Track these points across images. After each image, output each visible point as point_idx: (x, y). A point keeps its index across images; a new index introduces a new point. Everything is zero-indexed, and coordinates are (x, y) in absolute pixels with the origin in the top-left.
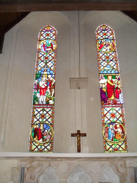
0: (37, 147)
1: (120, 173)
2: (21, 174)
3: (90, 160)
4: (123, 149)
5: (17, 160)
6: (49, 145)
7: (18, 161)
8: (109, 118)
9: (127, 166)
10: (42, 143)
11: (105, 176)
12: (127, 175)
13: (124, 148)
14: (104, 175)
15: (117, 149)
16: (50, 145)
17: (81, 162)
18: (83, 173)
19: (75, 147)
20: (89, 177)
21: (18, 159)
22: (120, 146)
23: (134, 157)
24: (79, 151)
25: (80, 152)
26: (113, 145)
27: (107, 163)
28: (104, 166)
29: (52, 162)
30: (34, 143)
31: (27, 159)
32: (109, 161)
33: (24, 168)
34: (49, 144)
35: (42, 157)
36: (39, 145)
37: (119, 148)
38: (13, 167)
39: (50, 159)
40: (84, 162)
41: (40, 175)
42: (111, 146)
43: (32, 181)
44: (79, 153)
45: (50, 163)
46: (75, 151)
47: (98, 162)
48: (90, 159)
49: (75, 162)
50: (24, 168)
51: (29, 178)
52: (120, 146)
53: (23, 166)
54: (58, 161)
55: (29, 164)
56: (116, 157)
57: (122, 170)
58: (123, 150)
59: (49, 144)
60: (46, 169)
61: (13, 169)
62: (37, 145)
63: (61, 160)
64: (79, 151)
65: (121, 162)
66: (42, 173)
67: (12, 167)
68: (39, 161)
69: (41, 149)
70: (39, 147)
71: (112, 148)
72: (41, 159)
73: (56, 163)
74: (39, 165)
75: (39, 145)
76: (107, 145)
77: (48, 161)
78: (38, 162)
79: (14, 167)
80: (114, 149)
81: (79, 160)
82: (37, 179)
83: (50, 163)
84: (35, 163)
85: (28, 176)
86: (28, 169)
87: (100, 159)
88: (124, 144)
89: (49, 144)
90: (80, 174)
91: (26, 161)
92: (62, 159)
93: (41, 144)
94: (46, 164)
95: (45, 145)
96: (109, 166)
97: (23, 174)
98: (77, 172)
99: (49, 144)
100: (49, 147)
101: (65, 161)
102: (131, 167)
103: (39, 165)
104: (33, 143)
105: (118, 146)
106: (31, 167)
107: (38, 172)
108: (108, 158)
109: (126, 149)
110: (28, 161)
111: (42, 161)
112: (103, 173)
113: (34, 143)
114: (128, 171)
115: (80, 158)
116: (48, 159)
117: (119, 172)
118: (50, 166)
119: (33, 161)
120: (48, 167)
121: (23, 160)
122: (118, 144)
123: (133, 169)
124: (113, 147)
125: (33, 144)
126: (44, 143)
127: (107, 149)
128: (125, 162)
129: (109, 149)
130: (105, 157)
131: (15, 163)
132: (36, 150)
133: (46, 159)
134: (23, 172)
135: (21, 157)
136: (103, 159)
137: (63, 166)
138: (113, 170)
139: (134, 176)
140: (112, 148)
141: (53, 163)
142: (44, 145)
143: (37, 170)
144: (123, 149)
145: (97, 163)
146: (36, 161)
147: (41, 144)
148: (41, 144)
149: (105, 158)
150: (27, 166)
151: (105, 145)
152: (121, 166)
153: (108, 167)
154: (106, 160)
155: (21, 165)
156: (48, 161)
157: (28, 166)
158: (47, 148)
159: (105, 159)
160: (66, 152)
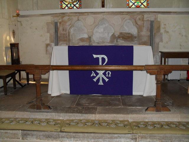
0: (67, 5)
1: (138, 25)
2: (55, 28)
3: (113, 14)
4: (144, 6)
5: (50, 17)
6: (77, 3)
7: (52, 17)
8: (142, 5)
9: (145, 19)
10: (71, 1)
11: (126, 27)
12: (144, 26)
13: (146, 6)
14: (124, 27)
15: (139, 6)
16: (78, 3)
17: (105, 16)
18: (107, 25)
19: (100, 3)
20: (112, 28)
21: (51, 15)
22: (142, 4)
23: (151, 12)
24: (103, 6)
25: (104, 7)
26: (135, 2)
27: (128, 17)
28: (125, 19)
29: (80, 17)
30: (64, 2)
31: (58, 15)
32: (129, 15)
33: (57, 23)
34: (77, 2)
35: (71, 13)
36: (68, 4)
37: (141, 5)
38: (48, 23)
39: (78, 14)
40: (107, 16)
41: (71, 27)
42: (134, 4)
43: (64, 32)
44: (103, 8)
45: (78, 17)
46: (100, 7)
47: (120, 16)
48: (112, 13)
49: (100, 16)
50: (57, 23)
51: (62, 30)
52: (142, 4)
53: (56, 21)
54: (85, 15)
55: (61, 19)
56: (135, 12)
57: (140, 23)
58: (144, 7)
59: (77, 2)
60: (76, 23)
61: (48, 24)
62: (67, 4)
63: (88, 15)
64: (103, 6)
65: (140, 16)
66: (72, 26)
67: (47, 23)
68: (69, 16)
69: (71, 7)
70: (69, 5)
71: (135, 5)
72: (71, 14)
73: (84, 17)
74: (69, 20)
75: (68, 4)
76: (130, 2)
77: (77, 16)
78: (68, 17)
79: (49, 22)
80: (137, 6)
81: (103, 14)
82: (69, 31)
83: (78, 17)
84: (66, 18)
85: (61, 29)
86: (60, 23)
87: (121, 13)
88: (146, 2)
89: (78, 2)
90: (104, 26)
91: (58, 17)
92: (89, 14)
93: (71, 3)
94: (75, 18)
95: (74, 4)
96: (129, 19)
97: (56, 27)
98: (102, 25)
99: (78, 2)
100: (77, 5)
101: (91, 15)
102: (148, 21)
103: (69, 20)
104: (63, 3)
105: (140, 4)
106: (62, 21)
107: (69, 25)
108: (128, 13)
109: (148, 6)
110: (59, 17)
111: (72, 16)
112: (123, 25)
113: (64, 2)
114: (145, 24)
115: (104, 12)
116: (77, 14)
117: (137, 24)
118: (78, 20)
119: (64, 17)
120: (77, 21)
121: (56, 16)
122: (140, 2)
123: (150, 22)
124: (136, 4)
125: (63, 3)
126: (72, 2)
127: (130, 6)
128: (143, 16)
129: (132, 6)
130: (125, 12)
131: (49, 19)
132: (67, 8)
133: (75, 14)
134: (56, 26)
135: (53, 14)
136: (124, 13)
137: (90, 20)
138: (133, 23)
139: (150, 27)
140: (135, 5)
141: (81, 17)
142: (73, 4)
143: (68, 24)
144: (144, 6)
145: (119, 17)
146: (66, 16)
147: (71, 3)
148: (70, 2)
149: (126, 12)
150: (60, 21)
151: (129, 2)
152: (139, 19)
153: (128, 20)
154: (127, 14)
155: (54, 20)
156: (77, 16)
157: (60, 21)
158: (76, 6)
159: (126, 13)
160: (92, 8)
